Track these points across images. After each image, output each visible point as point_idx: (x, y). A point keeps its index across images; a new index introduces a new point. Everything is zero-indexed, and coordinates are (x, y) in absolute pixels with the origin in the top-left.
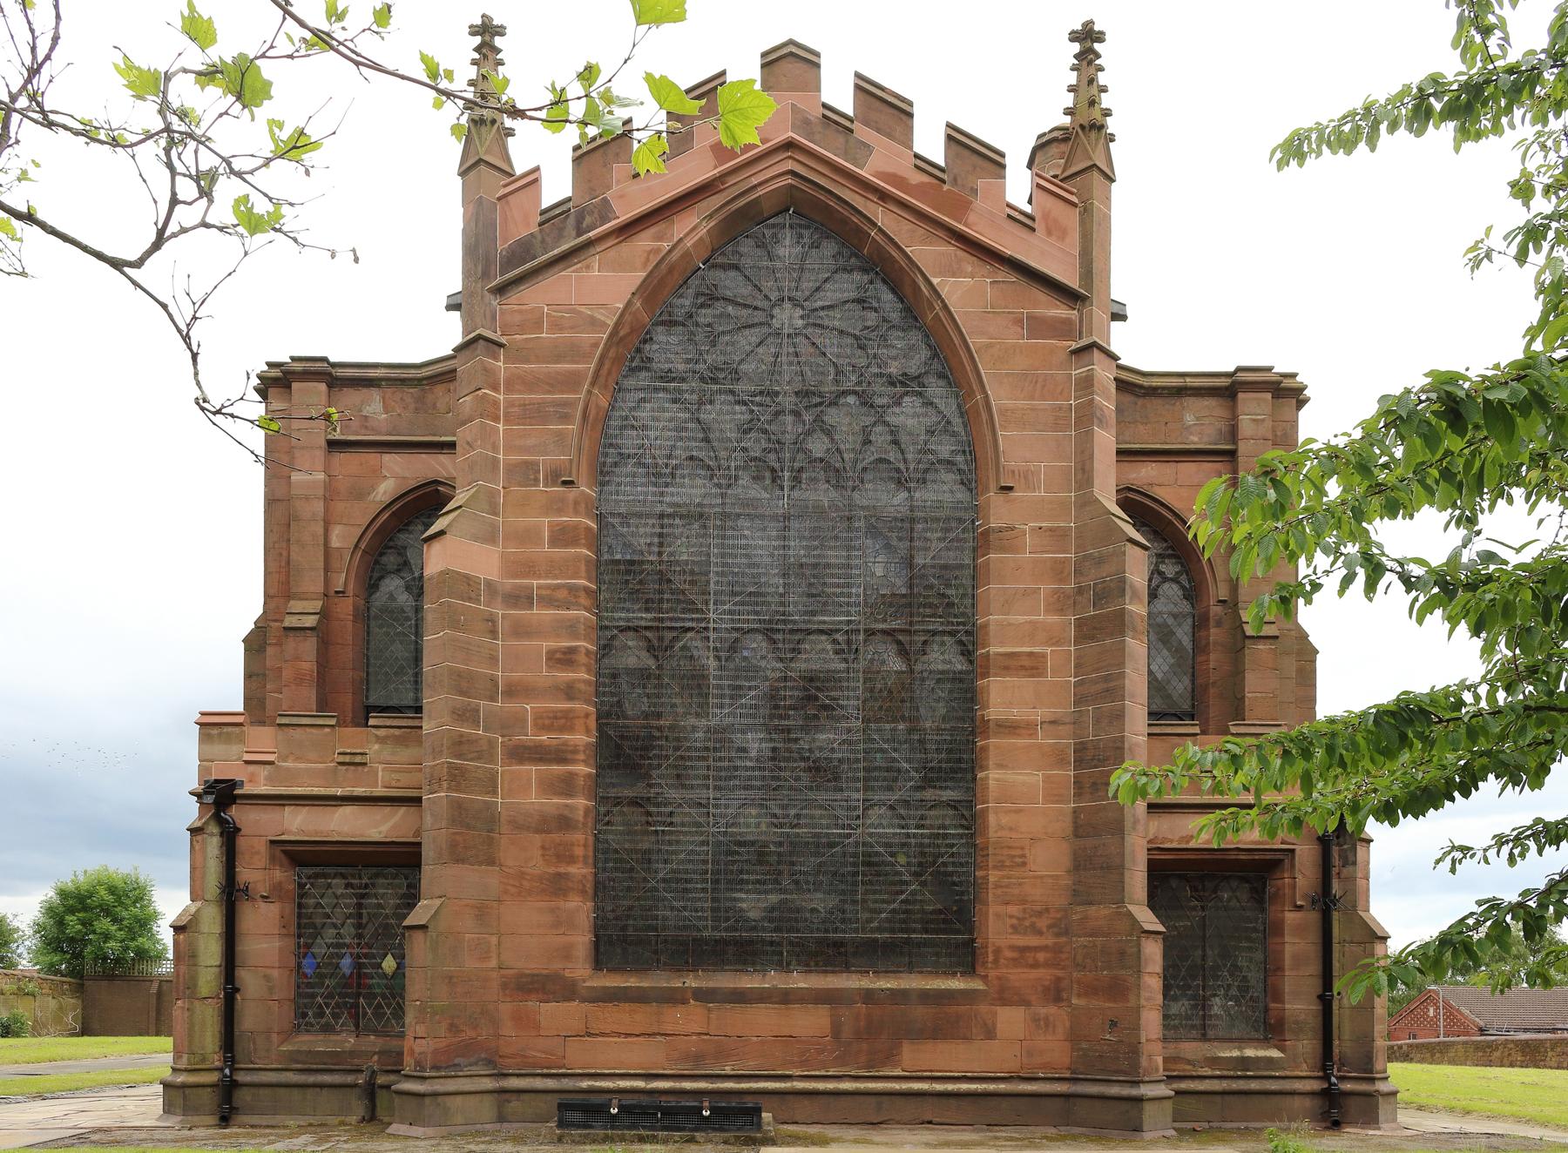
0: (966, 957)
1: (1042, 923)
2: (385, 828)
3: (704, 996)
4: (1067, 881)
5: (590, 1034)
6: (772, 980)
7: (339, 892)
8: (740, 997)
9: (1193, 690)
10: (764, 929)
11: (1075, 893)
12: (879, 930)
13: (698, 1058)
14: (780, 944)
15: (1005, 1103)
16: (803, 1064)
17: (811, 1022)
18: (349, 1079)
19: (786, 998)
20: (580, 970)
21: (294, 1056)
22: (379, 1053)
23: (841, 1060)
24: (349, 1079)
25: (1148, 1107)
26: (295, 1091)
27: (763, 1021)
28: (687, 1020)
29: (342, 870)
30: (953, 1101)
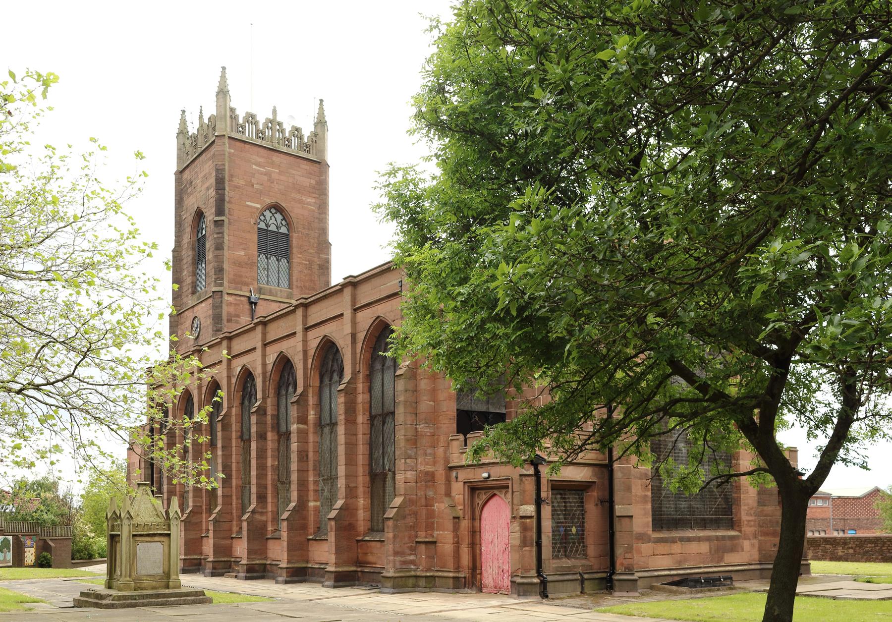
0: (732, 524)
1: (752, 512)
2: (581, 475)
3: (681, 539)
4: (756, 498)
5: (654, 555)
6: (690, 533)
7: (559, 500)
8: (689, 540)
9: (371, 402)
10: (686, 515)
11: (759, 502)
12: (712, 515)
13: (680, 562)
14: (691, 520)
15: (747, 573)
16: (704, 563)
17: (704, 547)
18: (575, 577)
19: (699, 539)
20: (649, 531)
21: (557, 569)
22: (582, 566)
23: (712, 561)
24: (575, 577)
25: (437, 579)
26: (560, 583)
27: (694, 548)
28: (677, 548)
29: (561, 492)
30: (740, 573)
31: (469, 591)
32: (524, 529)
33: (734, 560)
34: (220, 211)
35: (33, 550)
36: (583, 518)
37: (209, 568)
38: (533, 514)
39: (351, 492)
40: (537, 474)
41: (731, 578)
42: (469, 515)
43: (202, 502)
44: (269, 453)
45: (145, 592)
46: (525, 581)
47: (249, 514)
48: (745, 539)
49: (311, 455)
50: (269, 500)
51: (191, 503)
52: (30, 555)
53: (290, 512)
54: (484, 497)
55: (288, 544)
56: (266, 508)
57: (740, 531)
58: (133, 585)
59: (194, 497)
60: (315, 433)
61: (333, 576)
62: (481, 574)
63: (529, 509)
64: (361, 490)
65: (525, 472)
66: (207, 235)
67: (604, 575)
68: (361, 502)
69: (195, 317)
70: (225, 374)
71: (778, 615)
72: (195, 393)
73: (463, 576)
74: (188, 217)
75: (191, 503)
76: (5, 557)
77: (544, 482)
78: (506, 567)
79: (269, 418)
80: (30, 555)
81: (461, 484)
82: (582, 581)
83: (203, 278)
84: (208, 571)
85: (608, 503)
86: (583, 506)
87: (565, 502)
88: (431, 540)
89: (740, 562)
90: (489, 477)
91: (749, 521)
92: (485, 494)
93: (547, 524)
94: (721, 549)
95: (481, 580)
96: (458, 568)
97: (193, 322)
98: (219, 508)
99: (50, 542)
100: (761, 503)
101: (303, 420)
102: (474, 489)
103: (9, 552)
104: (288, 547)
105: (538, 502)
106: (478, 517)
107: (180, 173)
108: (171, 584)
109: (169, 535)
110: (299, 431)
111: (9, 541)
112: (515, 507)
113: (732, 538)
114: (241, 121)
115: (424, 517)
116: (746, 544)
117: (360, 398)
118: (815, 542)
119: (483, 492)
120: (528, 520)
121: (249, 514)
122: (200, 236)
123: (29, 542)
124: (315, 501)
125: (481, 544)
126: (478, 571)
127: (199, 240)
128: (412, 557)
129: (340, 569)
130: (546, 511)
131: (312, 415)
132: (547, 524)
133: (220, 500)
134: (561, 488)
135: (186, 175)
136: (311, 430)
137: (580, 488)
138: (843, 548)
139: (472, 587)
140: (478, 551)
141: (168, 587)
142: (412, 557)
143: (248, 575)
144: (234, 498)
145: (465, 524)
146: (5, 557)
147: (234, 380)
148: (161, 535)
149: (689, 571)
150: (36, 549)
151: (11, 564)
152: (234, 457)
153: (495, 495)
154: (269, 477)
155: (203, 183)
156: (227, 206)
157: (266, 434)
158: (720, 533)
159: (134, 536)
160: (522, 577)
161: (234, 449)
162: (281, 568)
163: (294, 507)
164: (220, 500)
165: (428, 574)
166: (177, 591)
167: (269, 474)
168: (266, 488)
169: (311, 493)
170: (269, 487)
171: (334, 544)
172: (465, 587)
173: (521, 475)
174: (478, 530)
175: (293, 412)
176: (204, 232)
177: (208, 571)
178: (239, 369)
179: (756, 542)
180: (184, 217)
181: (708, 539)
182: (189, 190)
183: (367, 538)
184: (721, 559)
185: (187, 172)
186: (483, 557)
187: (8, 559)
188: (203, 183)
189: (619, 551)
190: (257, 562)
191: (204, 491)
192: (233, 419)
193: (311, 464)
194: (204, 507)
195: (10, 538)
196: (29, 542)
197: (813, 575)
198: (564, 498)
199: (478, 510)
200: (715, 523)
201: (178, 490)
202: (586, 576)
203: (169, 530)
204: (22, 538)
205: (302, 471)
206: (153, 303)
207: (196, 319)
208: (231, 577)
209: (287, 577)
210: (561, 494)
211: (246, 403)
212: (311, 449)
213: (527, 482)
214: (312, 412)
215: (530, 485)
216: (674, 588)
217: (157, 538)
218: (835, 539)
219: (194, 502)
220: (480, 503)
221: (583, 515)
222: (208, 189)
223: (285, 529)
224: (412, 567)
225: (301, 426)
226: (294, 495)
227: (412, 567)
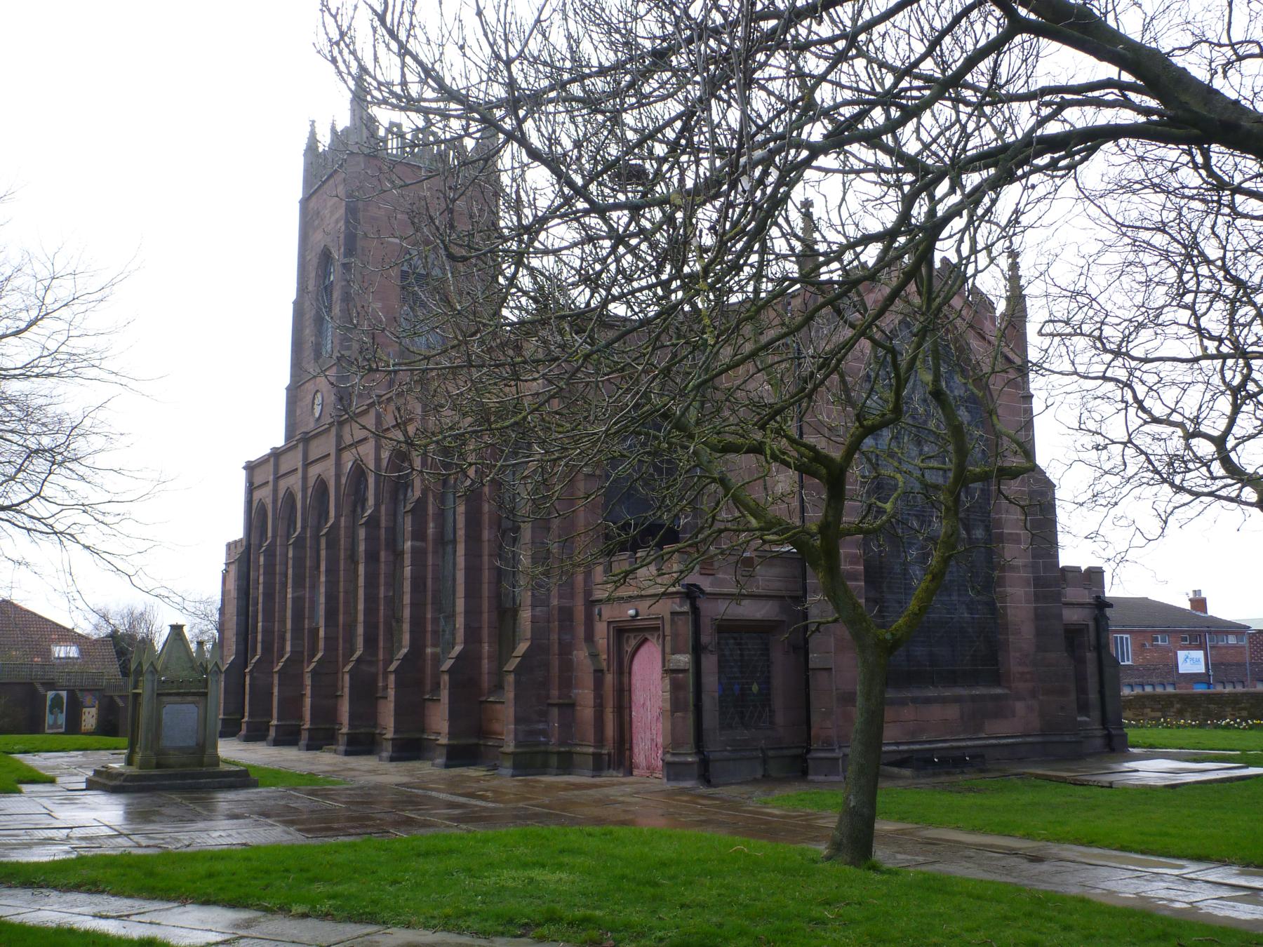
0: (997, 678)
3: (915, 700)
6: (931, 692)
8: (928, 701)
17: (952, 712)
19: (944, 701)
27: (936, 713)
29: (735, 635)
31: (615, 773)
32: (676, 687)
33: (1001, 731)
34: (350, 250)
35: (94, 711)
36: (769, 672)
37: (304, 741)
38: (690, 666)
39: (472, 634)
40: (695, 610)
41: (982, 756)
42: (614, 667)
43: (304, 646)
45: (170, 771)
46: (676, 759)
47: (397, 657)
51: (288, 648)
52: (90, 718)
53: (453, 661)
54: (633, 642)
55: (395, 705)
56: (376, 655)
58: (154, 761)
59: (292, 639)
60: (435, 552)
61: (444, 751)
62: (631, 749)
63: (684, 660)
64: (485, 633)
65: (678, 609)
66: (335, 283)
67: (799, 751)
69: (317, 391)
70: (332, 472)
71: (854, 807)
72: (299, 496)
73: (606, 752)
74: (313, 258)
75: (288, 648)
76: (56, 720)
77: (706, 623)
78: (660, 740)
79: (383, 531)
80: (90, 718)
81: (605, 624)
82: (765, 761)
83: (329, 338)
84: (303, 742)
85: (801, 649)
87: (740, 649)
88: (566, 701)
90: (637, 614)
92: (635, 638)
93: (711, 681)
95: (631, 757)
96: (600, 740)
97: (314, 399)
98: (320, 655)
99: (118, 700)
101: (419, 534)
102: (621, 631)
103: (62, 712)
104: (395, 710)
105: (698, 651)
106: (626, 670)
107: (305, 203)
108: (205, 759)
109: (205, 694)
110: (414, 550)
111: (61, 698)
112: (668, 657)
113: (997, 698)
114: (382, 132)
115: (557, 670)
116: (1020, 706)
118: (1140, 702)
119: (632, 635)
120: (681, 675)
121: (397, 657)
122: (327, 283)
123: (88, 699)
124: (434, 645)
125: (630, 708)
126: (627, 746)
127: (326, 288)
128: (541, 726)
129: (455, 742)
130: (710, 663)
131: (431, 528)
132: (711, 681)
133: (321, 644)
134: (728, 628)
135: (313, 204)
136: (430, 549)
137: (762, 629)
138: (1233, 709)
139: (619, 768)
140: (627, 718)
141: (201, 764)
142: (541, 726)
143: (349, 749)
144: (341, 641)
145: (609, 678)
146: (56, 720)
147: (343, 480)
148: (194, 694)
149: (927, 746)
150: (99, 710)
151: (63, 730)
152: (342, 584)
153: (645, 640)
155: (332, 213)
156: (359, 244)
159: (159, 695)
160: (673, 754)
161: (342, 573)
162: (386, 739)
163: (406, 655)
164: (321, 644)
165: (562, 749)
166: (211, 769)
167: (382, 608)
168: (377, 627)
169: (429, 636)
170: (381, 626)
171: (447, 706)
172: (609, 768)
173: (673, 613)
174: (626, 688)
175: (408, 524)
176: (332, 278)
177: (303, 742)
178: (350, 464)
180: (309, 258)
181: (958, 700)
182: (316, 223)
183: (491, 699)
185: (314, 199)
186: (634, 726)
187: (59, 722)
188: (332, 213)
189: (815, 719)
190: (362, 730)
191: (296, 594)
192: (342, 532)
194: (306, 654)
195: (64, 694)
196: (88, 699)
198: (740, 644)
199: (626, 659)
200: (972, 678)
201: (276, 629)
202: (771, 753)
203: (206, 687)
204: (79, 694)
205: (417, 605)
207: (319, 395)
208: (330, 751)
209: (393, 752)
210: (735, 639)
211: (359, 510)
213: (680, 622)
214: (431, 525)
215: (686, 628)
216: (896, 770)
217: (190, 699)
218: (1221, 695)
219: (292, 646)
220: (629, 650)
221: (768, 666)
222: (337, 222)
223: (393, 686)
224: (542, 739)
225: (418, 544)
226: (406, 638)
227: (542, 739)
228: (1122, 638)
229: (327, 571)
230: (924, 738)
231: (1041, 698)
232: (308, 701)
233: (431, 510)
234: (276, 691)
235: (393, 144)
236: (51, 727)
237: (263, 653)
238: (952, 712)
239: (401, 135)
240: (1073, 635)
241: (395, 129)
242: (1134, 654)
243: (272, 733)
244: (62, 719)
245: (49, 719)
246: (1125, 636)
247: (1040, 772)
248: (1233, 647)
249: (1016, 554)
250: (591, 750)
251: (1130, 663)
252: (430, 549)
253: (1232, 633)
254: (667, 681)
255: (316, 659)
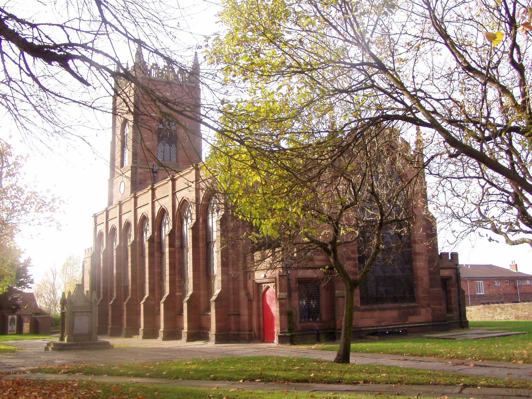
0: (413, 299)
3: (379, 309)
6: (385, 306)
8: (384, 309)
13: (379, 323)
19: (391, 309)
20: (359, 305)
28: (377, 314)
35: (28, 324)
44: (156, 264)
48: (422, 307)
49: (177, 265)
50: (156, 292)
51: (115, 295)
52: (26, 327)
57: (419, 303)
68: (202, 292)
75: (115, 295)
79: (156, 244)
80: (26, 327)
86: (319, 292)
89: (422, 320)
91: (424, 297)
94: (405, 315)
100: (431, 286)
109: (91, 312)
113: (413, 307)
114: (149, 68)
117: (201, 233)
124: (179, 292)
133: (130, 292)
136: (177, 251)
150: (31, 323)
151: (15, 333)
154: (156, 278)
157: (154, 253)
158: (404, 305)
159: (73, 312)
164: (130, 292)
179: (429, 309)
184: (407, 320)
193: (177, 270)
196: (26, 319)
197: (471, 328)
200: (403, 299)
202: (320, 332)
203: (91, 309)
204: (22, 317)
206: (412, 14)
212: (177, 262)
217: (85, 314)
228: (479, 283)
229: (131, 261)
230: (384, 324)
231: (432, 306)
232: (125, 317)
233: (177, 235)
234: (110, 313)
235: (153, 72)
236: (10, 331)
237: (103, 297)
238: (395, 314)
239: (158, 69)
240: (445, 281)
241: (155, 67)
242: (485, 289)
243: (109, 331)
244: (15, 327)
245: (10, 328)
246: (481, 282)
247: (428, 336)
248: (529, 286)
249: (420, 247)
250: (248, 333)
251: (483, 293)
252: (177, 251)
253: (528, 279)
254: (278, 303)
255: (128, 299)
